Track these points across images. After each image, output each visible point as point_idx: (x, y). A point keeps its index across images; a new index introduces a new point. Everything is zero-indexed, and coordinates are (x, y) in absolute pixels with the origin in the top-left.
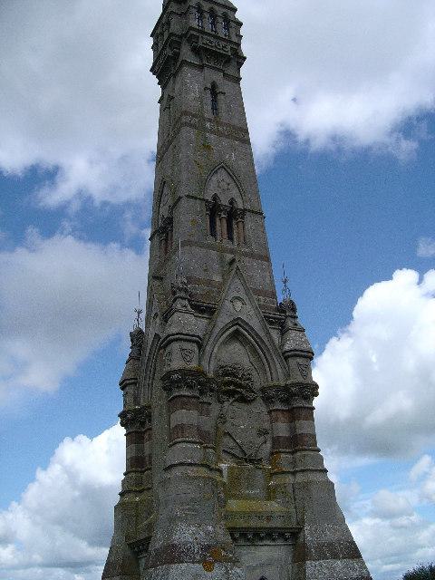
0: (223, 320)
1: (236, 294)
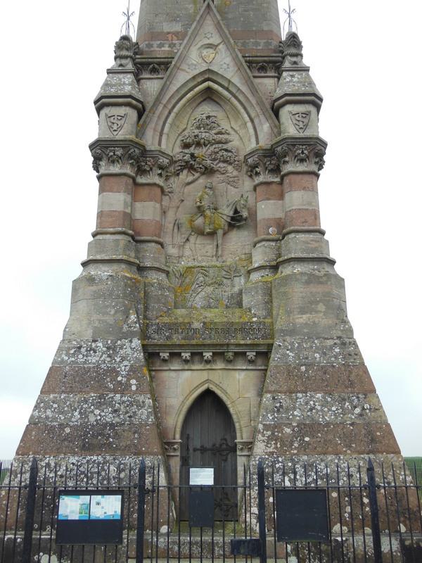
0: (182, 78)
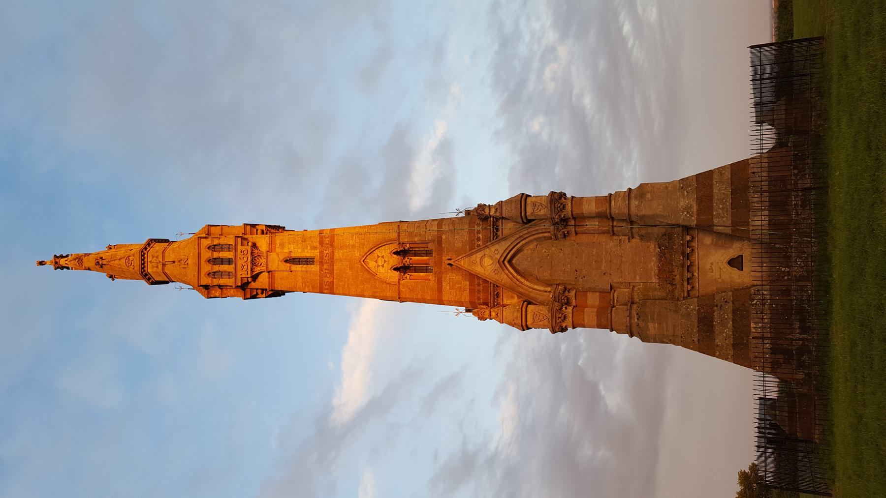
1: (478, 260)
